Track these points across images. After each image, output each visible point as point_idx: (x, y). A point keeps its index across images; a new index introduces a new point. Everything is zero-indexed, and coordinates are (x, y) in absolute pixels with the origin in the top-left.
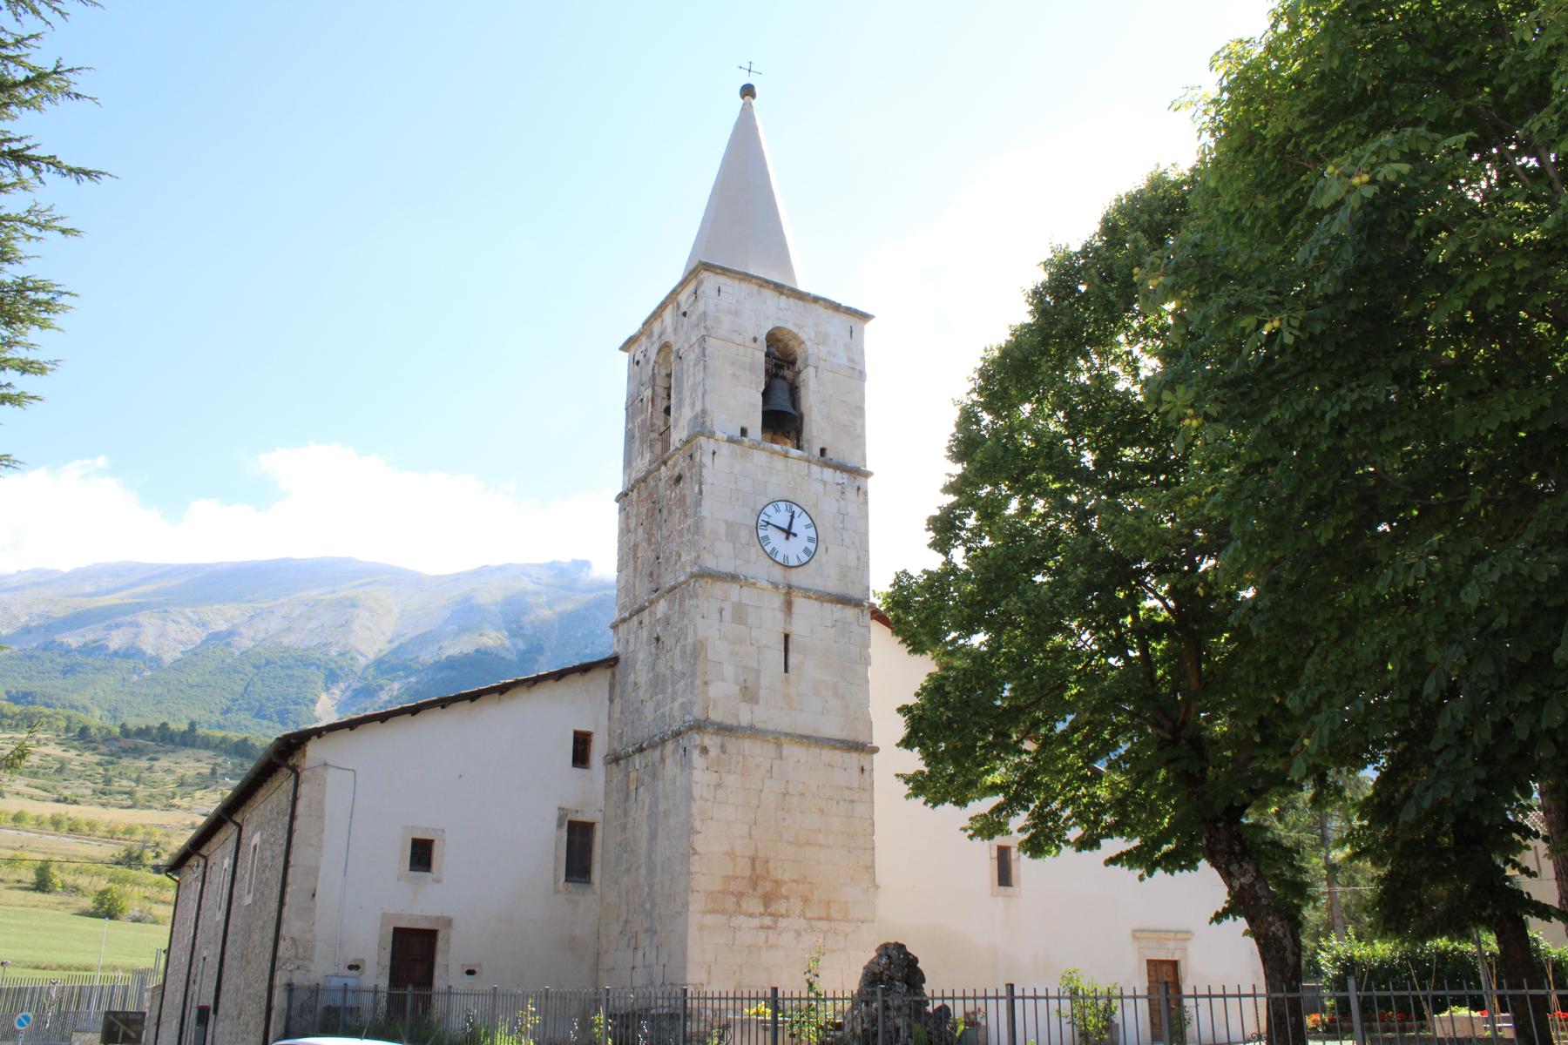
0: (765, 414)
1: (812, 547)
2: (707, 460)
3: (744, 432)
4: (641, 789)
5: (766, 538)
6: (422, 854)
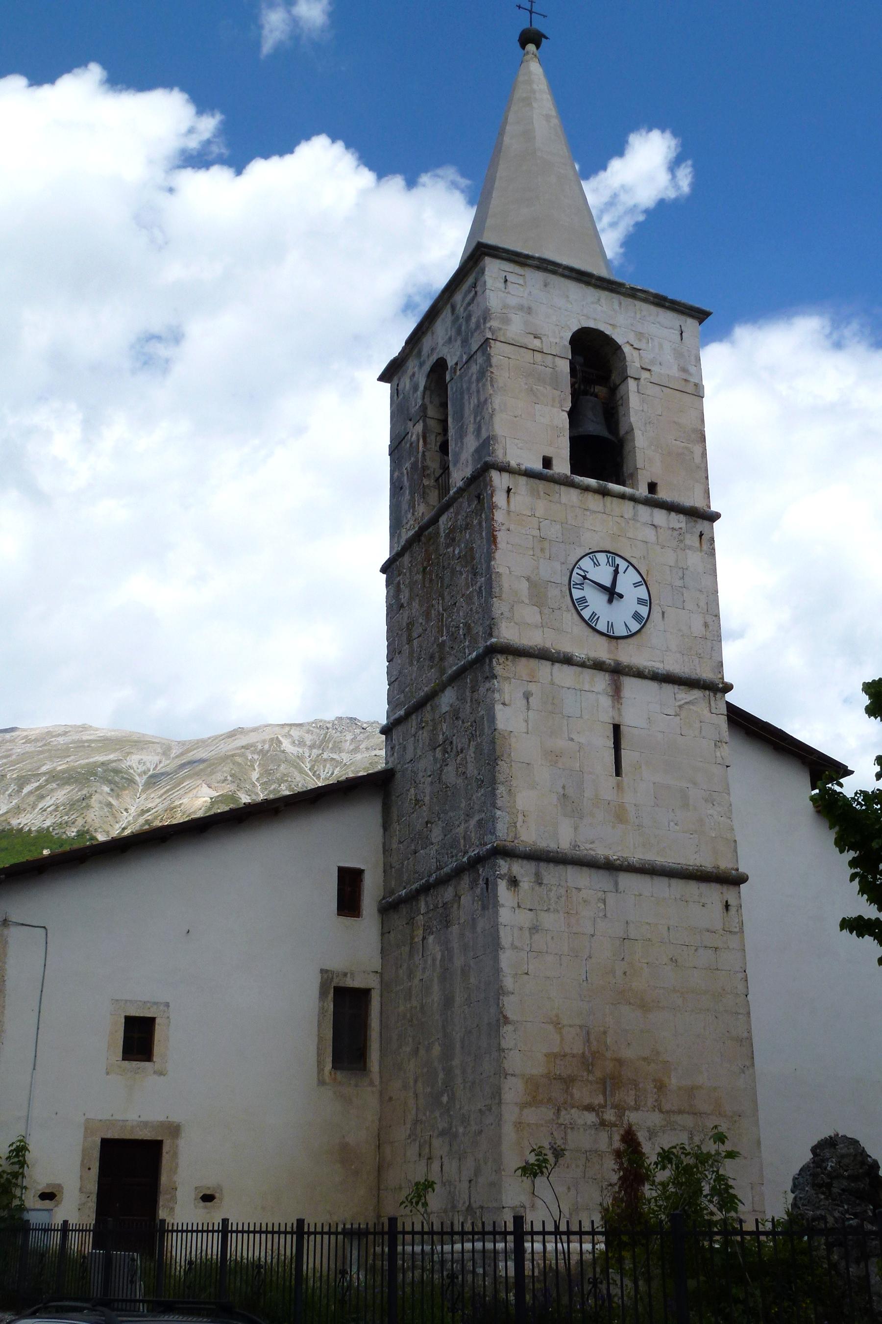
0: (573, 440)
1: (644, 611)
2: (500, 499)
3: (547, 462)
4: (431, 939)
5: (583, 600)
6: (138, 1038)
